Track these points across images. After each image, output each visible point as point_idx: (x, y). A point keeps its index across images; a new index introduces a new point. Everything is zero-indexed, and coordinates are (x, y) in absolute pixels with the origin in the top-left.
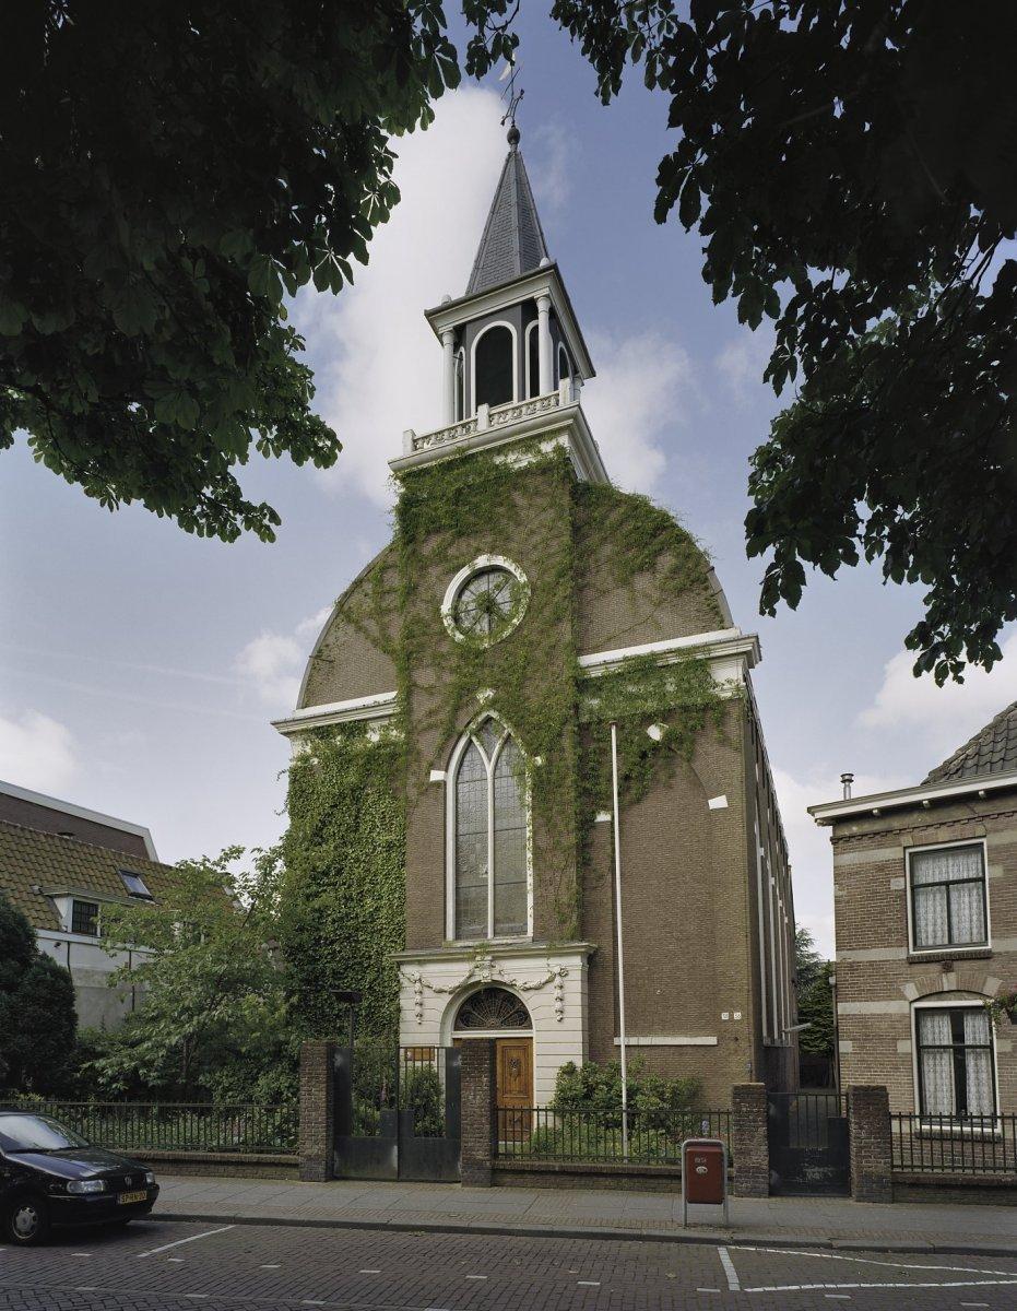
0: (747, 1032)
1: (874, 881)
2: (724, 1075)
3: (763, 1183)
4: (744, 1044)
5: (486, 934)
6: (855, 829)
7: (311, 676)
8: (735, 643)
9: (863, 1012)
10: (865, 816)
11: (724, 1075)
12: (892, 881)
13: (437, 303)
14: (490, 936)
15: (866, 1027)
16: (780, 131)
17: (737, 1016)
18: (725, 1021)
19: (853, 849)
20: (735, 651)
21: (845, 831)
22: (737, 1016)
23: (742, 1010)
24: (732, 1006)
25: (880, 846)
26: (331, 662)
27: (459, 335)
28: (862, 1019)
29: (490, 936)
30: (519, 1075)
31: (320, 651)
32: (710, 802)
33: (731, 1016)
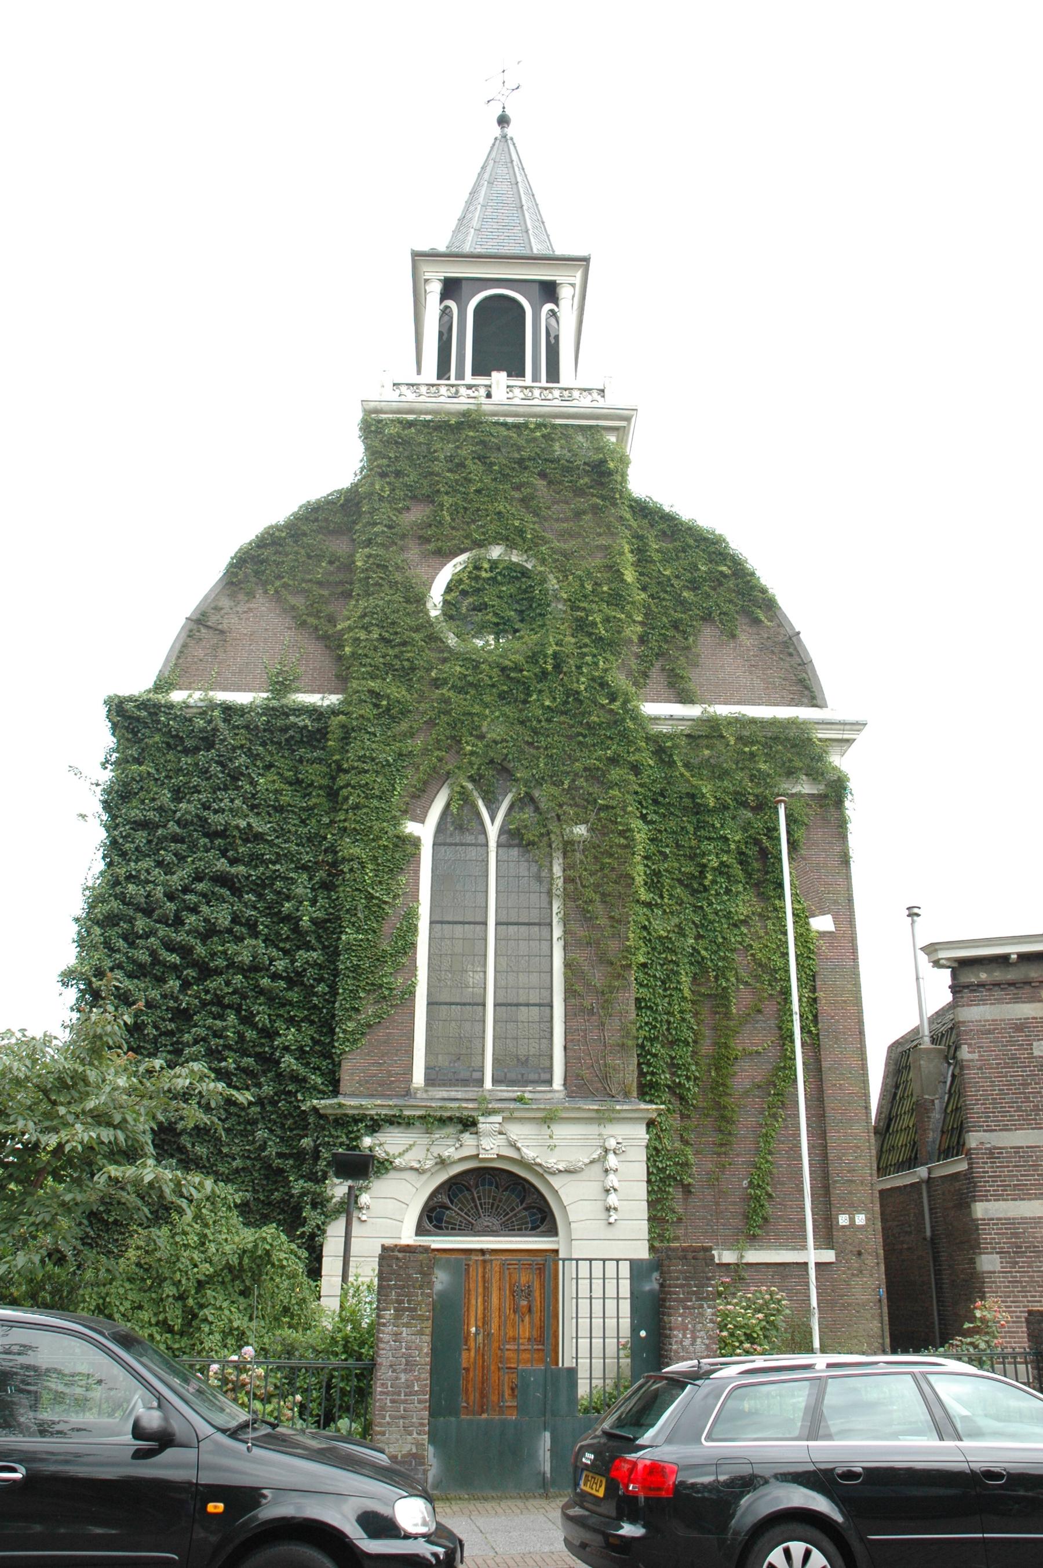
0: (875, 1243)
1: (1012, 1043)
2: (844, 1307)
3: (677, 1271)
4: (870, 1261)
5: (481, 1082)
6: (983, 976)
7: (185, 646)
8: (842, 727)
9: (1010, 1215)
10: (1003, 960)
11: (844, 1307)
12: (1035, 1043)
13: (425, 248)
14: (488, 1084)
15: (1015, 1235)
16: (269, 826)
17: (860, 1219)
18: (844, 1227)
19: (983, 1001)
20: (840, 737)
21: (971, 977)
22: (860, 1219)
23: (865, 1210)
24: (852, 1205)
25: (1017, 1000)
26: (222, 632)
27: (451, 288)
28: (1010, 1223)
29: (488, 1084)
30: (530, 1310)
31: (204, 614)
32: (812, 920)
33: (852, 1220)
